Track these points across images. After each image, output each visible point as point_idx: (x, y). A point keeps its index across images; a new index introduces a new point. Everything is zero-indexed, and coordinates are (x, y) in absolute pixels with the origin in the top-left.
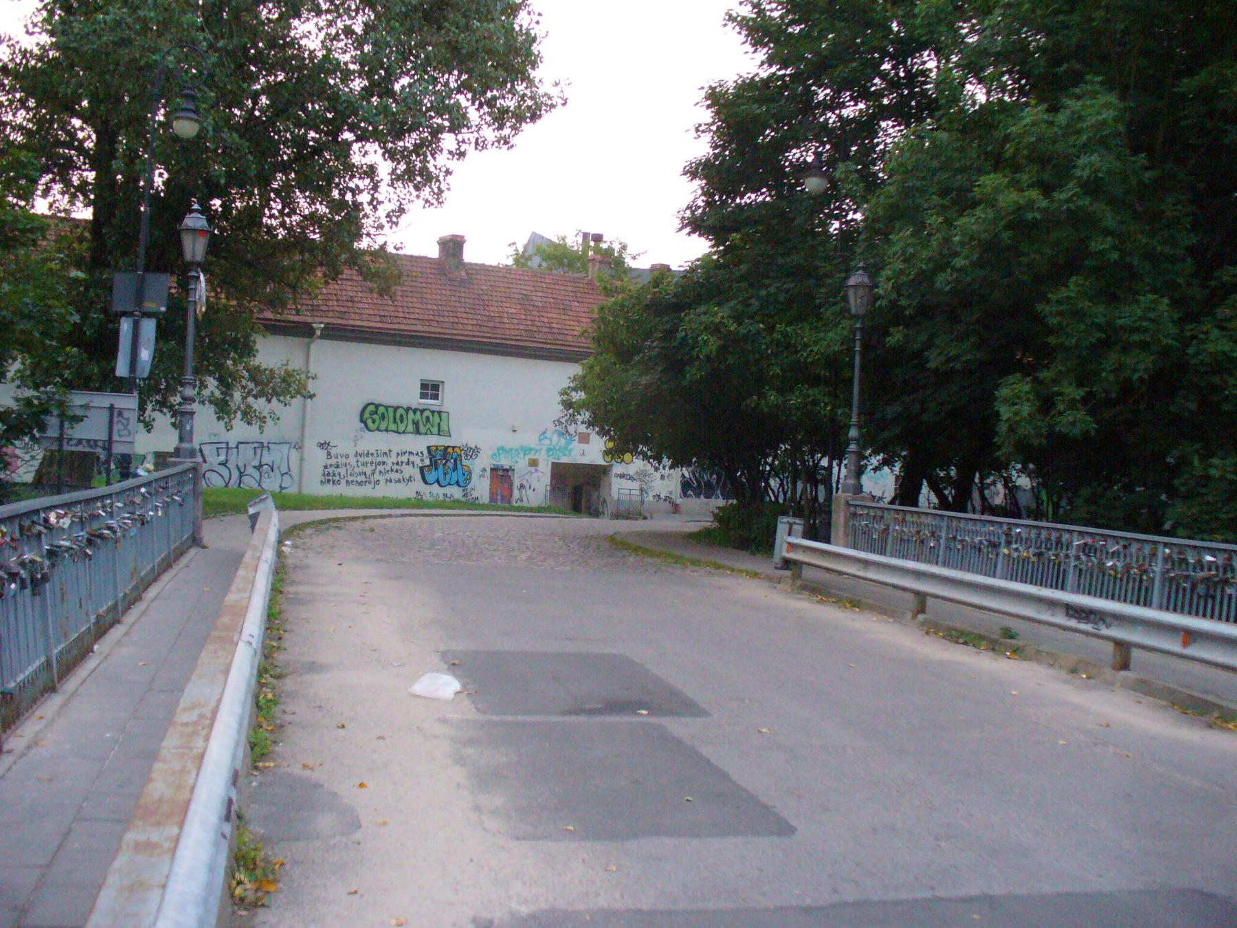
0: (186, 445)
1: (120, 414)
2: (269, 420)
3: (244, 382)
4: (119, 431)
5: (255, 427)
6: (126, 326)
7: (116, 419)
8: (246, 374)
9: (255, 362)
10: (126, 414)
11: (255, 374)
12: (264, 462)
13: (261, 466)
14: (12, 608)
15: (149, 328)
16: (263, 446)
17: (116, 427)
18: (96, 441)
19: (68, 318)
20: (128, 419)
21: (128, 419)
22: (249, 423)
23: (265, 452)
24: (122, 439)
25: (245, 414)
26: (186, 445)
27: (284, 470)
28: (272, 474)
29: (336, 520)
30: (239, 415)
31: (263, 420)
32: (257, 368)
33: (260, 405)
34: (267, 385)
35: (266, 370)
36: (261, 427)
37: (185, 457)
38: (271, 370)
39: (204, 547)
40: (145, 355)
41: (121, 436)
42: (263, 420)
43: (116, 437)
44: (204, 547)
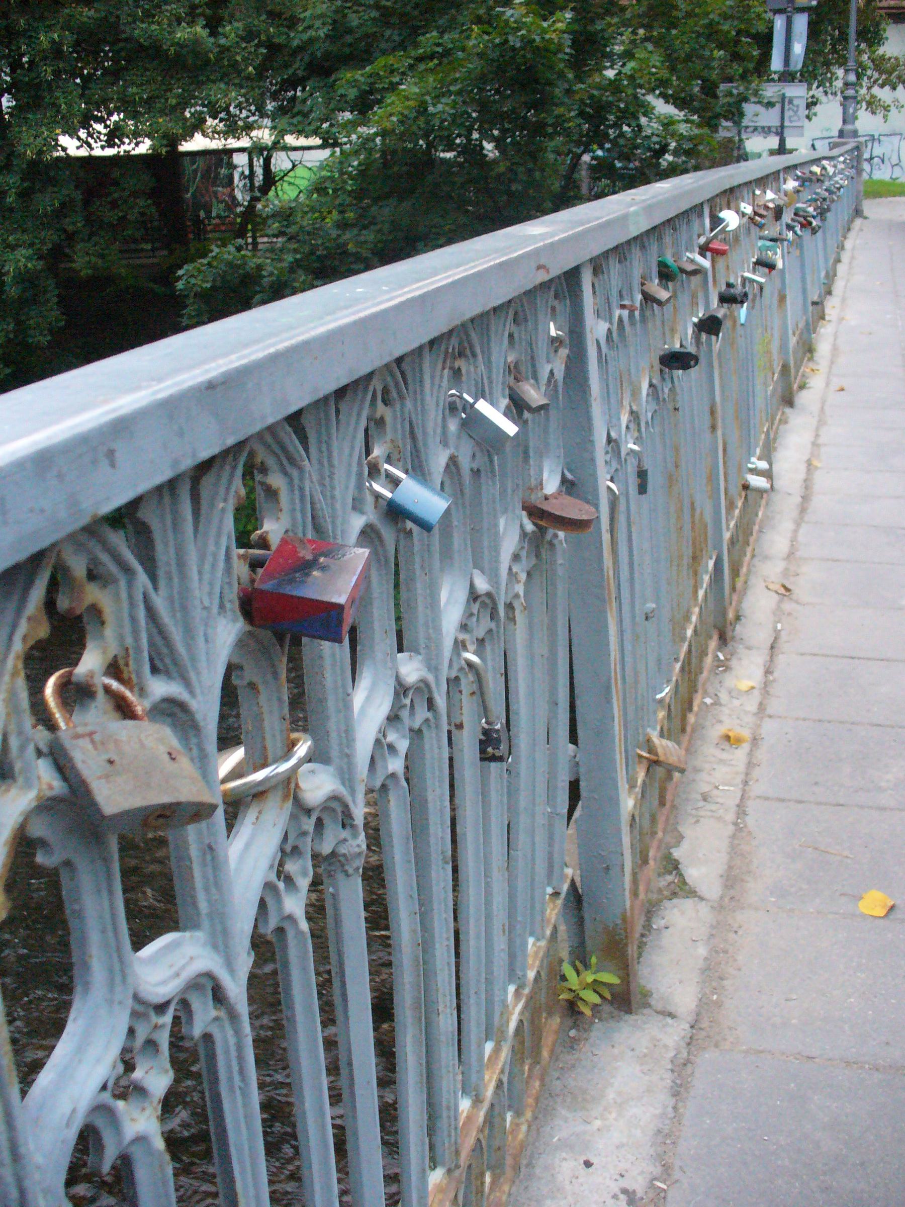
0: (849, 127)
1: (790, 102)
2: (893, 109)
3: (869, 72)
4: (790, 117)
5: (879, 117)
6: (779, 23)
7: (786, 107)
8: (870, 64)
9: (881, 51)
10: (796, 102)
11: (879, 64)
12: (874, 155)
13: (871, 158)
14: (355, 412)
15: (801, 23)
16: (874, 140)
17: (787, 114)
18: (769, 128)
19: (764, 15)
20: (798, 106)
21: (798, 106)
22: (873, 113)
23: (876, 144)
24: (794, 124)
25: (869, 104)
26: (849, 127)
27: (895, 161)
28: (882, 166)
29: (313, 517)
30: (864, 104)
31: (887, 109)
32: (882, 58)
33: (884, 94)
34: (891, 74)
35: (890, 58)
36: (885, 117)
37: (849, 137)
38: (896, 59)
39: (866, 218)
40: (798, 49)
41: (791, 121)
42: (887, 109)
43: (787, 123)
44: (866, 218)
